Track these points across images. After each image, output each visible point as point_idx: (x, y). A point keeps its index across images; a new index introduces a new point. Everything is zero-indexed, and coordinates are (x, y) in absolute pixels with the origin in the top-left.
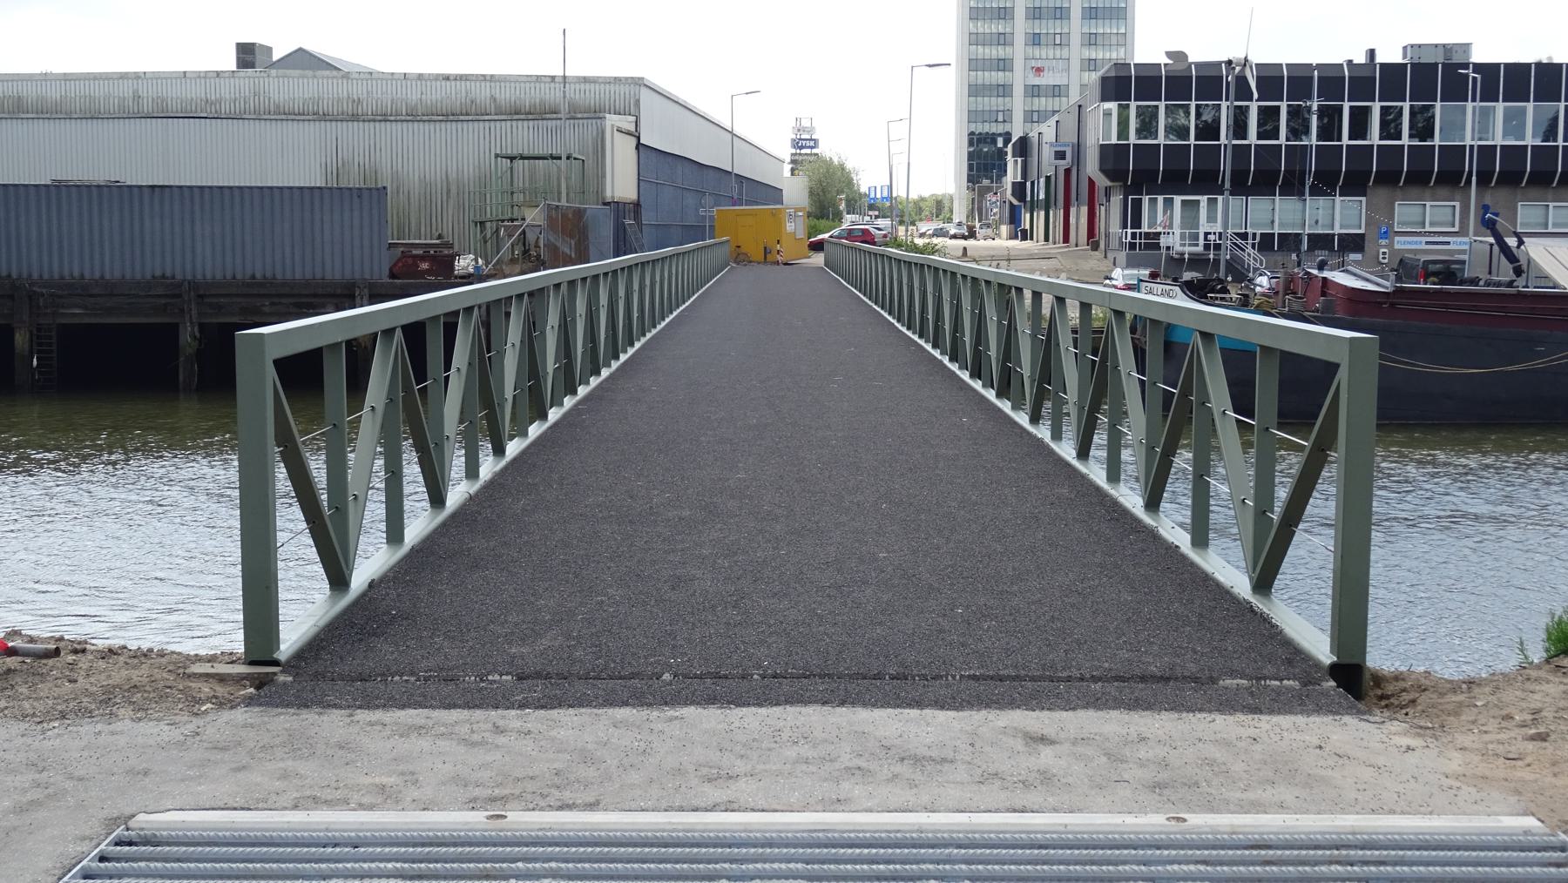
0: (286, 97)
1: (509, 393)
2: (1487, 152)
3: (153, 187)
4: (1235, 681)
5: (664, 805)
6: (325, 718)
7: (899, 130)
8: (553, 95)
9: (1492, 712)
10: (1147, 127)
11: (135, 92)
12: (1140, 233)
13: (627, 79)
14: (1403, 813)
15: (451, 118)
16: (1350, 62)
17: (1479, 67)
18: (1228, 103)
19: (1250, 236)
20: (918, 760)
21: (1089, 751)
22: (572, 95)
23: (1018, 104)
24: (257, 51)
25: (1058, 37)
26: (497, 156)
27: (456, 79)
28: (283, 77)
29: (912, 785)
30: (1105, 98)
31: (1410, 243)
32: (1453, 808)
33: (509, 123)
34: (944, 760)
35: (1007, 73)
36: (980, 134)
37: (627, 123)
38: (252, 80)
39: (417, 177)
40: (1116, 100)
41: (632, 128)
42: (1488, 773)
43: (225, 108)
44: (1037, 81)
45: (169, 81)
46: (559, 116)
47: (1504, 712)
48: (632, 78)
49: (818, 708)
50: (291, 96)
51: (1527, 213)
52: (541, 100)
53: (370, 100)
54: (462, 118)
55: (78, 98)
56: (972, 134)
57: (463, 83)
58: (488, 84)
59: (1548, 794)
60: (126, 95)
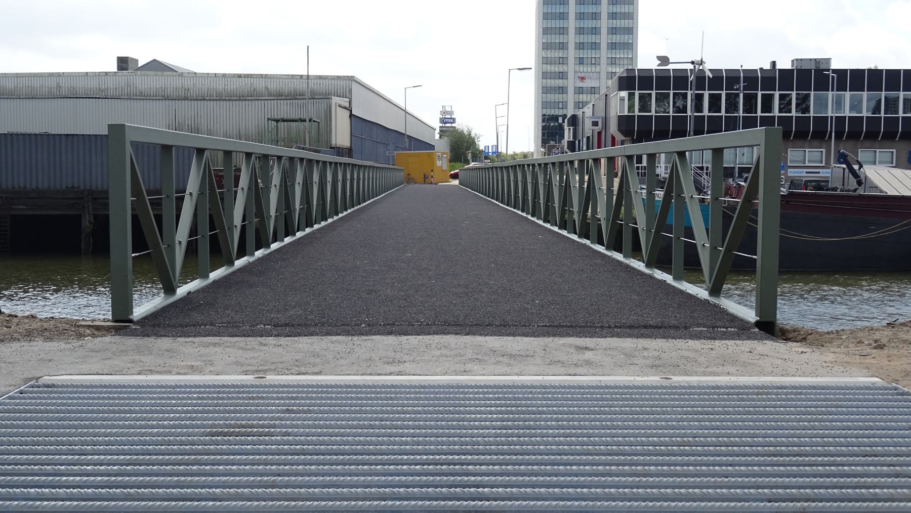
0: (146, 87)
1: (273, 212)
2: (840, 120)
3: (67, 135)
4: (700, 329)
5: (361, 373)
6: (159, 340)
7: (502, 110)
8: (301, 86)
9: (851, 341)
10: (645, 106)
11: (58, 84)
12: (642, 167)
13: (344, 77)
14: (799, 376)
15: (242, 98)
16: (761, 69)
17: (834, 71)
18: (692, 92)
19: (705, 169)
20: (511, 356)
21: (614, 353)
22: (313, 86)
23: (571, 98)
25: (593, 59)
26: (268, 119)
27: (245, 77)
28: (144, 75)
29: (509, 365)
30: (621, 88)
31: (796, 172)
32: (830, 374)
33: (275, 101)
34: (527, 356)
35: (564, 80)
36: (549, 115)
37: (344, 102)
38: (126, 77)
39: (222, 132)
40: (627, 90)
41: (347, 105)
42: (849, 361)
43: (110, 93)
44: (581, 85)
45: (78, 77)
46: (305, 97)
47: (858, 340)
48: (347, 76)
49: (453, 336)
50: (149, 86)
51: (863, 154)
52: (294, 89)
53: (195, 88)
54: (248, 98)
55: (24, 88)
56: (544, 115)
57: (249, 79)
58: (264, 79)
59: (885, 368)
60: (52, 86)
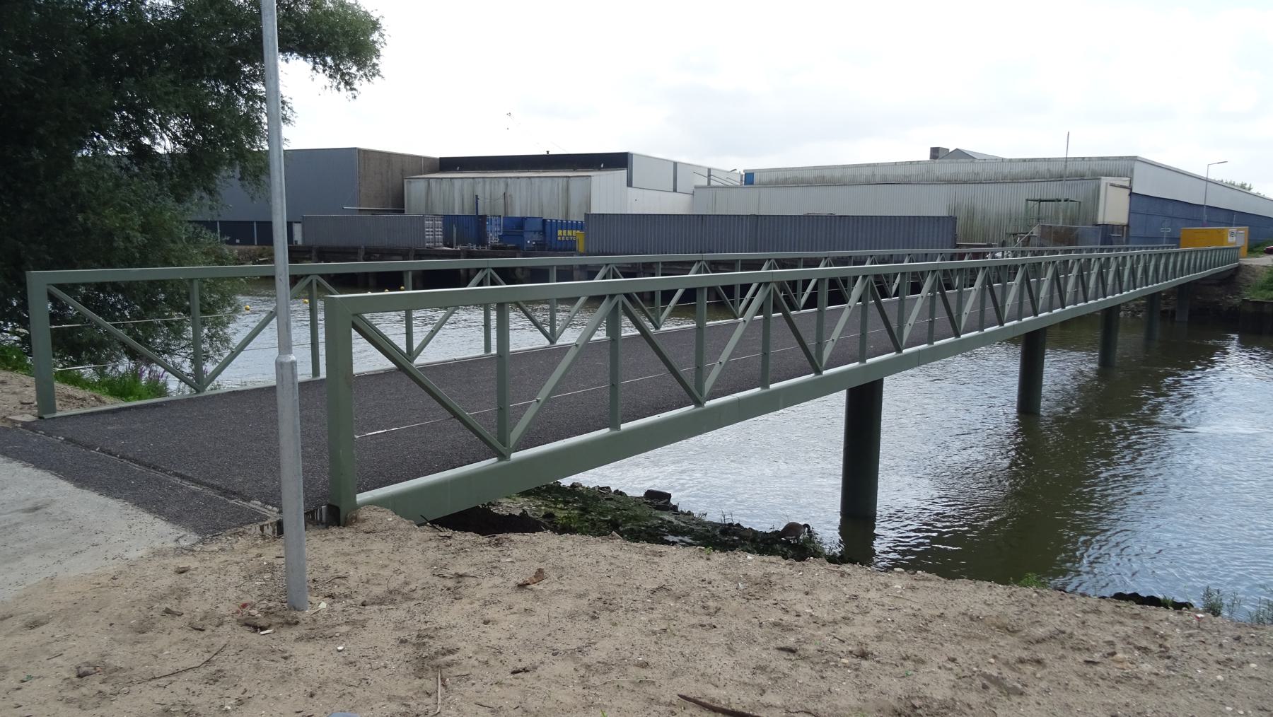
24: (940, 152)
